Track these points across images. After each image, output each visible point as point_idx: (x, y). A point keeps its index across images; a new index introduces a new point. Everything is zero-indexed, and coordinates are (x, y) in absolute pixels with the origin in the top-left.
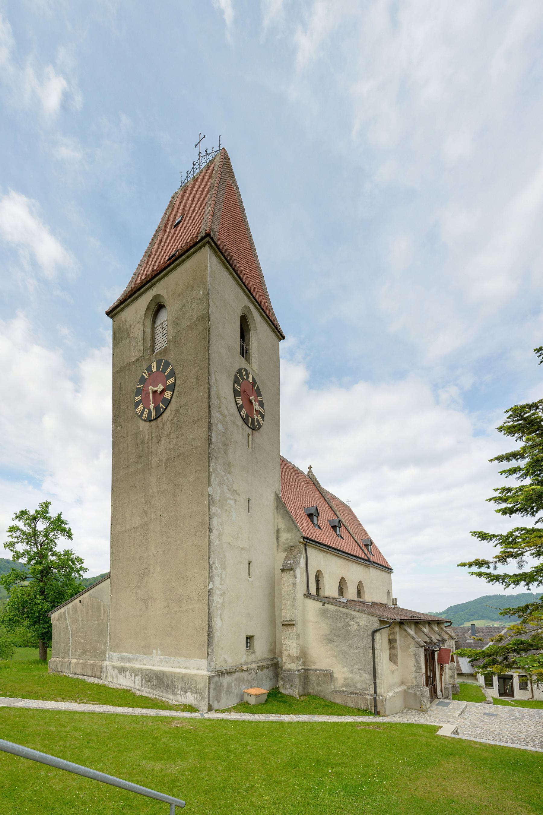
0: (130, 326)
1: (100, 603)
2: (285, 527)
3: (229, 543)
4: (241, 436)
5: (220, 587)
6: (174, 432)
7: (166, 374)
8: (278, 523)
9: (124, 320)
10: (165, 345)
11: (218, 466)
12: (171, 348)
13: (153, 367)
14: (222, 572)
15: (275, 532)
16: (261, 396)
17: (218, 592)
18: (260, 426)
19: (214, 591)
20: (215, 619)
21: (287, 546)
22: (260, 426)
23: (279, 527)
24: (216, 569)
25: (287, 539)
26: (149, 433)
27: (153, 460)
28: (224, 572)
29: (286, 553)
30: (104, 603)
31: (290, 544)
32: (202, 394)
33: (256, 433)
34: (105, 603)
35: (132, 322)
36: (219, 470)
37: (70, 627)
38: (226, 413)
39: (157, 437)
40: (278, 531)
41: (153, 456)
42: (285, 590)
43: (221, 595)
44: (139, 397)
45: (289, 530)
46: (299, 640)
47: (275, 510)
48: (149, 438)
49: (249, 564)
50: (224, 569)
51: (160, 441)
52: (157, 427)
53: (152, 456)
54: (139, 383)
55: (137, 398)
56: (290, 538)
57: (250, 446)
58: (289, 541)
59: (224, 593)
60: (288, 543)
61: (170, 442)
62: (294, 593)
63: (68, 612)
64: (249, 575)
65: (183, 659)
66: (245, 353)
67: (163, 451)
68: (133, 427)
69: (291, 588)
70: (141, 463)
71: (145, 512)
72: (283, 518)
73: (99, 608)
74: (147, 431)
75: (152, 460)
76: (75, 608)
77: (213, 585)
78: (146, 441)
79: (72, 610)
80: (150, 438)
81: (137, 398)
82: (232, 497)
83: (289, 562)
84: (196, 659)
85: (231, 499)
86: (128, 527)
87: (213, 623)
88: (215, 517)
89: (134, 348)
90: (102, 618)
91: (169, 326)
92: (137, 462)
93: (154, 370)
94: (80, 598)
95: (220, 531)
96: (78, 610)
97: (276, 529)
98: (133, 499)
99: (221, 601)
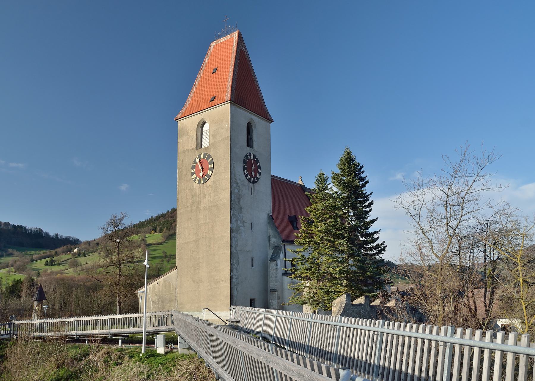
0: (189, 130)
1: (171, 284)
2: (273, 235)
3: (241, 250)
4: (247, 190)
5: (236, 274)
6: (213, 193)
7: (209, 161)
8: (269, 232)
9: (185, 125)
10: (208, 145)
11: (235, 212)
12: (211, 149)
13: (201, 155)
14: (237, 266)
15: (268, 237)
16: (259, 162)
17: (235, 277)
18: (258, 179)
19: (233, 277)
20: (234, 291)
21: (274, 246)
22: (258, 179)
23: (270, 235)
24: (234, 265)
25: (274, 242)
26: (199, 191)
27: (202, 206)
28: (238, 266)
29: (273, 250)
30: (173, 284)
31: (276, 245)
32: (227, 125)
33: (256, 184)
34: (174, 284)
35: (190, 128)
36: (235, 214)
37: (151, 299)
38: (239, 182)
39: (203, 194)
40: (269, 237)
41: (201, 203)
42: (272, 272)
43: (237, 278)
44: (193, 170)
45: (275, 237)
46: (279, 300)
47: (268, 224)
48: (199, 193)
49: (252, 259)
50: (238, 264)
51: (205, 196)
52: (203, 188)
53: (201, 203)
54: (194, 162)
55: (193, 170)
56: (275, 241)
57: (252, 193)
58: (275, 243)
59: (238, 277)
60: (275, 244)
61: (211, 197)
62: (276, 274)
63: (149, 290)
64: (252, 265)
65: (218, 312)
66: (249, 143)
67: (207, 202)
68: (190, 186)
69: (275, 271)
70: (194, 206)
71: (197, 233)
72: (272, 229)
73: (170, 287)
74: (198, 190)
75: (201, 206)
76: (154, 287)
77: (232, 274)
78: (198, 194)
79: (152, 289)
80: (200, 193)
81: (193, 170)
82: (242, 225)
83: (274, 256)
84: (225, 312)
85: (242, 226)
86: (187, 241)
87: (233, 293)
88: (234, 239)
89: (191, 142)
90: (172, 293)
91: (210, 136)
92: (192, 205)
93: (202, 157)
94: (157, 281)
95: (236, 245)
96: (157, 288)
97: (268, 235)
98: (190, 226)
99: (237, 281)
